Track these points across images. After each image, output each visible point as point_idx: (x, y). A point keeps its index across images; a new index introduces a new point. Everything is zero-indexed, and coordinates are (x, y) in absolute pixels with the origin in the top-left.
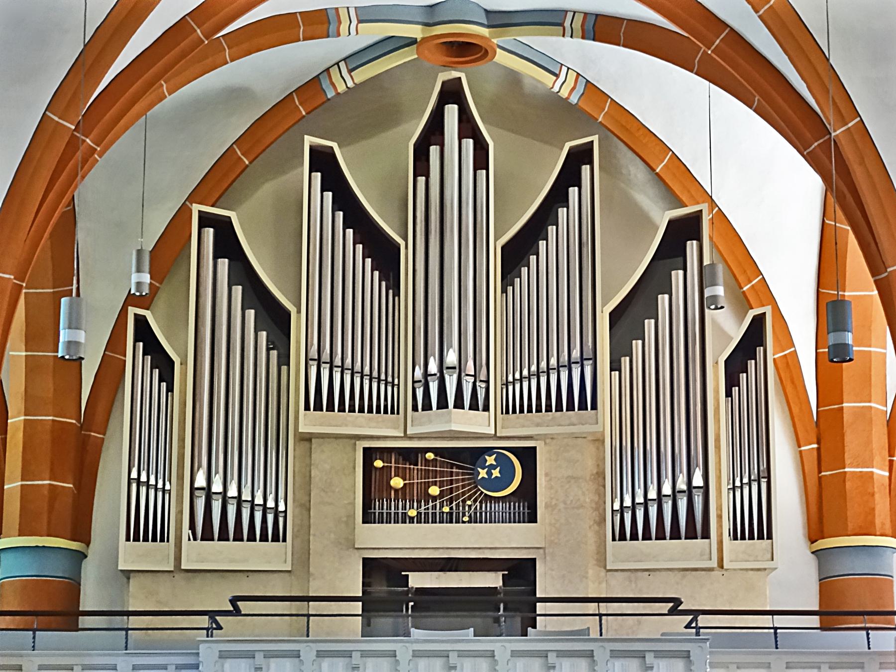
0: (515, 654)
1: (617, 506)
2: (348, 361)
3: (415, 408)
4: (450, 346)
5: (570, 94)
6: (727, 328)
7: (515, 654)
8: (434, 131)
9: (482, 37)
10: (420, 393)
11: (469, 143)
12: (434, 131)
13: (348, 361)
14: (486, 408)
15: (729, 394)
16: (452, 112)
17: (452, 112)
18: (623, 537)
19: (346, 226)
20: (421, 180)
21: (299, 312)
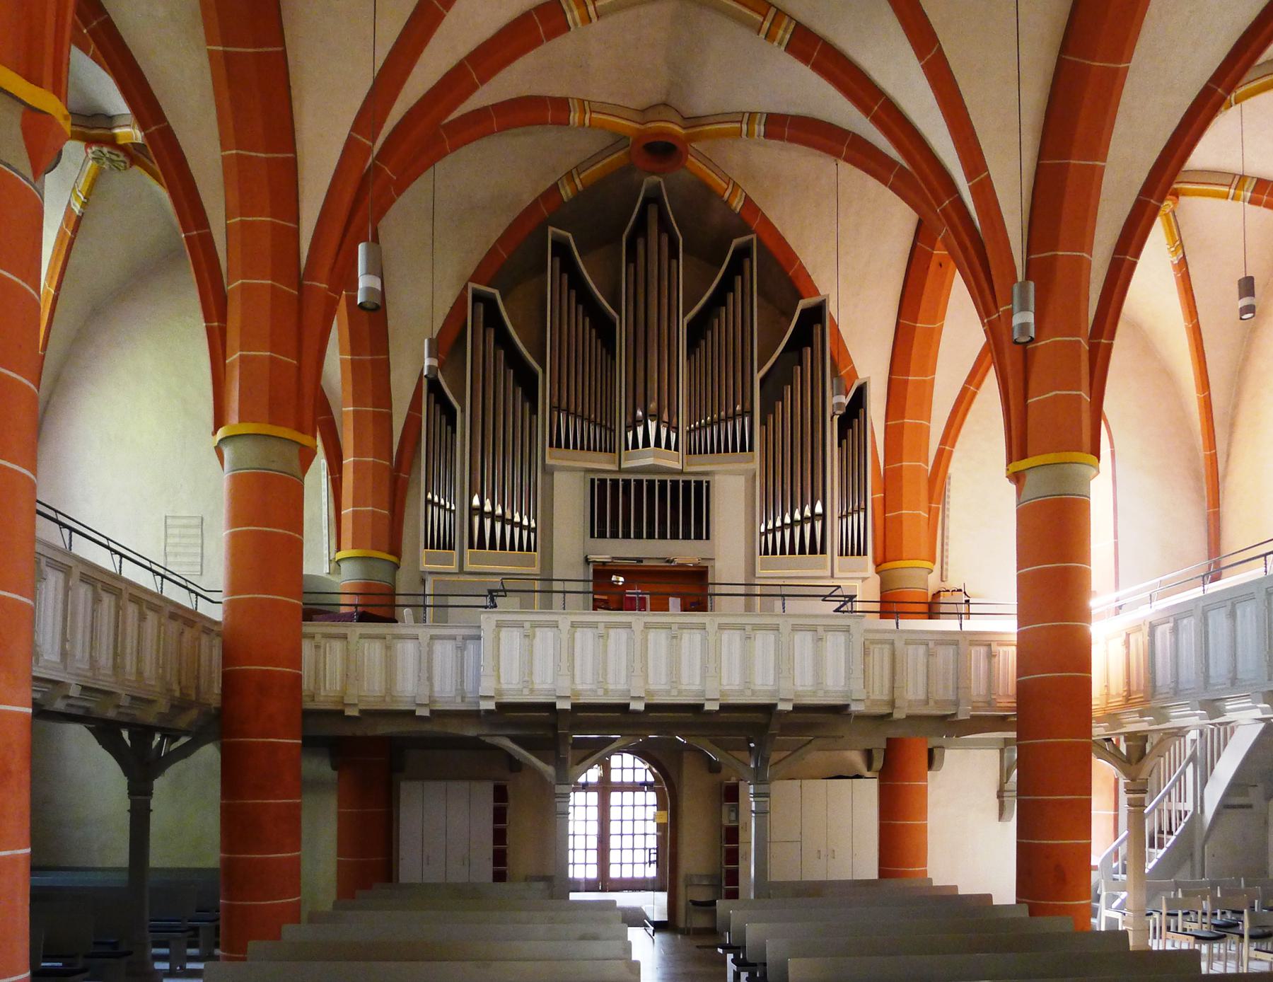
0: (362, 636)
1: (763, 530)
2: (580, 409)
3: (627, 449)
4: (652, 399)
5: (703, 677)
6: (838, 401)
7: (362, 636)
8: (641, 227)
9: (676, 137)
10: (630, 435)
11: (665, 238)
12: (641, 227)
13: (580, 409)
14: (676, 449)
15: (840, 445)
16: (653, 211)
17: (653, 211)
18: (766, 553)
19: (577, 302)
20: (632, 266)
21: (544, 372)
